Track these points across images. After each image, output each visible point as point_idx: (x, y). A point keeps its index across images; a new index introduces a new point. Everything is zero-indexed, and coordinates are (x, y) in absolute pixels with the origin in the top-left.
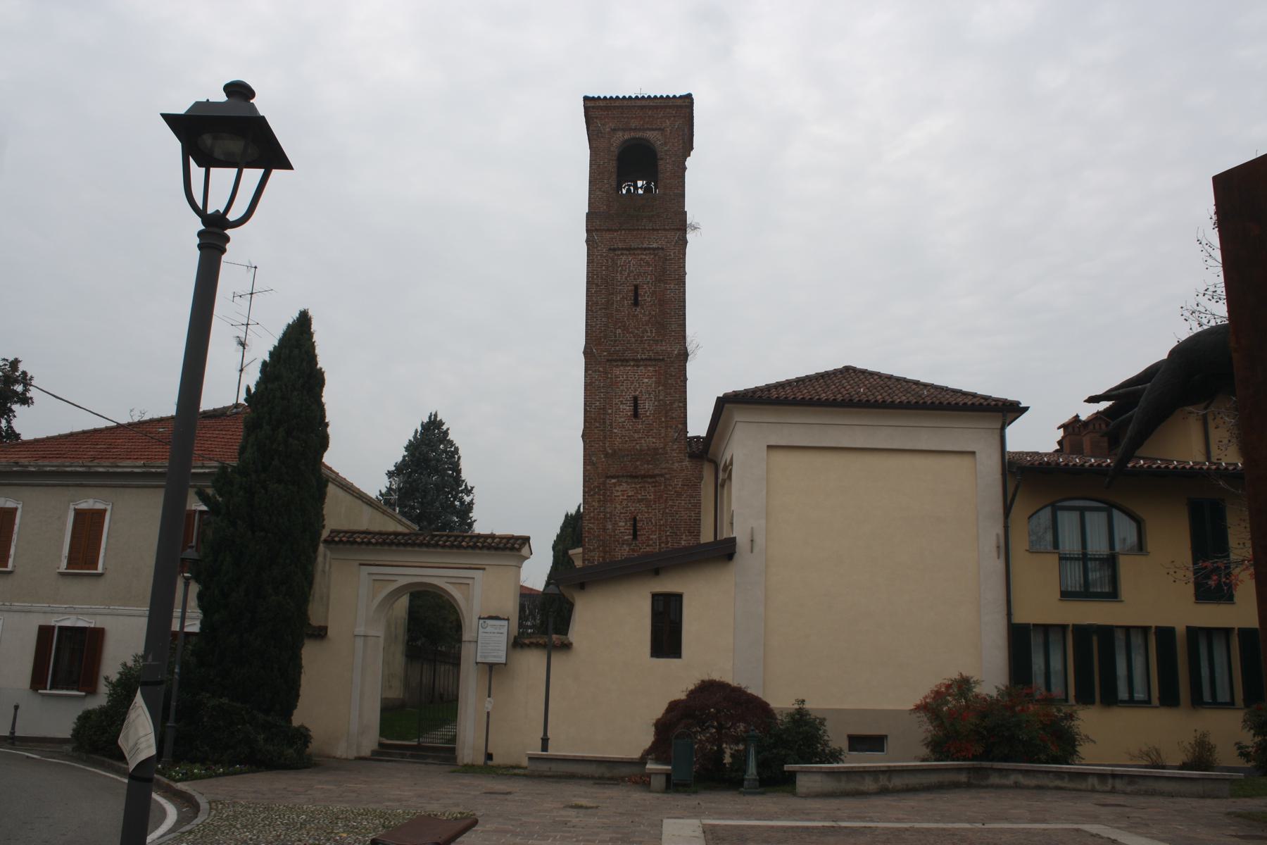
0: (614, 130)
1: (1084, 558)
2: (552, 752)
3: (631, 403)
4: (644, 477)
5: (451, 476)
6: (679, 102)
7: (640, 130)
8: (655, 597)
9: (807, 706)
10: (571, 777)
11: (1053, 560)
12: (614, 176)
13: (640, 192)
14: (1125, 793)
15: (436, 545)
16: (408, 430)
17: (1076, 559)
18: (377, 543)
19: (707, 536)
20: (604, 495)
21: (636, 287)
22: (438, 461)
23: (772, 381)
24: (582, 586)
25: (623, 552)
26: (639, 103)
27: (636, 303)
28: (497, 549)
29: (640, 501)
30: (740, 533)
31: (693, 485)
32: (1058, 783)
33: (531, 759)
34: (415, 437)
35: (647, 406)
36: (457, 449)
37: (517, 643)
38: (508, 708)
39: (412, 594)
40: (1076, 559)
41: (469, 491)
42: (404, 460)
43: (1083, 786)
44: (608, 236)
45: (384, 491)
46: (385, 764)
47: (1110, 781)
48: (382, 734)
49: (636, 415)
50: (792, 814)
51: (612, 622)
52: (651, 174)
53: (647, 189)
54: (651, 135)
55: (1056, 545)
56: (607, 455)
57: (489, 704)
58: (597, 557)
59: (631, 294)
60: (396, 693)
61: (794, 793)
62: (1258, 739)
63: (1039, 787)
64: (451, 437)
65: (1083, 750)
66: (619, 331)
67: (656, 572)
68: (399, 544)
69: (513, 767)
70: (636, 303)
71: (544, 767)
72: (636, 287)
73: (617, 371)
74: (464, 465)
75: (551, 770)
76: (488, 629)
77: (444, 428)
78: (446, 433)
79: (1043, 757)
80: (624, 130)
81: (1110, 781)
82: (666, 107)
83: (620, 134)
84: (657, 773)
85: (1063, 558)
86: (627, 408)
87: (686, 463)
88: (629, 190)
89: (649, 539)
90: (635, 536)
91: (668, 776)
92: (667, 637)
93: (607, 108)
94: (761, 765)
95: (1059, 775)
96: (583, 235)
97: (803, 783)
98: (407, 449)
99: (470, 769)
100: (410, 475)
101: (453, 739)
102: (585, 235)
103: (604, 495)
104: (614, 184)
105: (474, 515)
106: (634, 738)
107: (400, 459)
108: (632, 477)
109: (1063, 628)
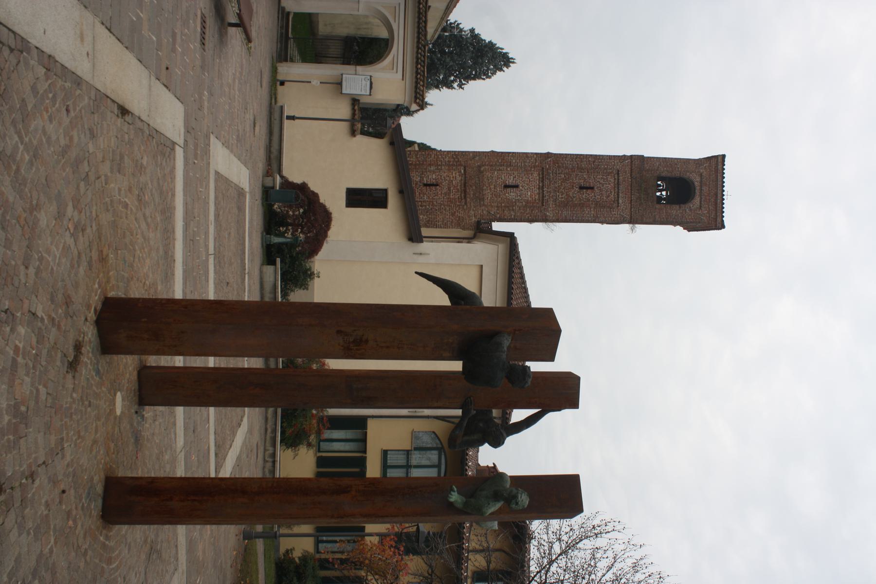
0: (701, 175)
1: (408, 467)
2: (287, 123)
3: (514, 183)
4: (465, 191)
5: (471, 72)
6: (719, 220)
7: (701, 192)
8: (385, 191)
9: (316, 279)
10: (270, 133)
11: (408, 447)
12: (669, 175)
13: (658, 194)
14: (264, 468)
15: (418, 48)
16: (503, 44)
17: (408, 461)
18: (419, 8)
19: (425, 232)
20: (453, 165)
21: (592, 188)
22: (482, 64)
23: (526, 271)
24: (392, 143)
25: (415, 177)
26: (719, 192)
27: (581, 188)
28: (416, 87)
29: (449, 189)
30: (425, 246)
31: (459, 224)
32: (269, 430)
33: (282, 107)
34: (499, 48)
35: (512, 194)
36: (490, 77)
37: (355, 101)
38: (314, 95)
39: (388, 40)
40: (408, 461)
41: (461, 86)
42: (482, 40)
43: (268, 444)
44: (628, 169)
45: (461, 26)
46: (276, 15)
47: (271, 460)
48: (296, 14)
49: (506, 187)
50: (252, 253)
51: (368, 163)
52: (670, 200)
53: (660, 198)
54: (697, 200)
55: (416, 449)
56: (480, 167)
57: (315, 83)
58: (412, 159)
59: (588, 185)
60: (323, 29)
61: (262, 265)
62: (297, 560)
63: (266, 430)
64: (498, 73)
65: (289, 452)
66: (563, 176)
67: (401, 192)
68: (419, 23)
69: (276, 99)
70: (581, 188)
71: (276, 115)
72: (592, 188)
73: (535, 174)
74: (478, 82)
75: (275, 120)
76: (364, 82)
77: (505, 69)
78: (501, 70)
79: (285, 425)
80: (701, 182)
81: (271, 460)
82: (716, 210)
83: (698, 179)
84: (274, 180)
85: (408, 453)
86: (510, 181)
87: (474, 219)
88: (660, 186)
89: (424, 194)
90: (426, 185)
91: (273, 188)
92: (359, 198)
93: (717, 171)
94: (280, 245)
95: (274, 431)
96: (628, 153)
97: (269, 269)
98: (490, 42)
99: (274, 71)
100: (472, 44)
101: (292, 61)
102: (629, 154)
103: (453, 165)
104: (664, 174)
105: (445, 90)
106: (295, 170)
107: (483, 37)
108: (465, 183)
109: (365, 452)
